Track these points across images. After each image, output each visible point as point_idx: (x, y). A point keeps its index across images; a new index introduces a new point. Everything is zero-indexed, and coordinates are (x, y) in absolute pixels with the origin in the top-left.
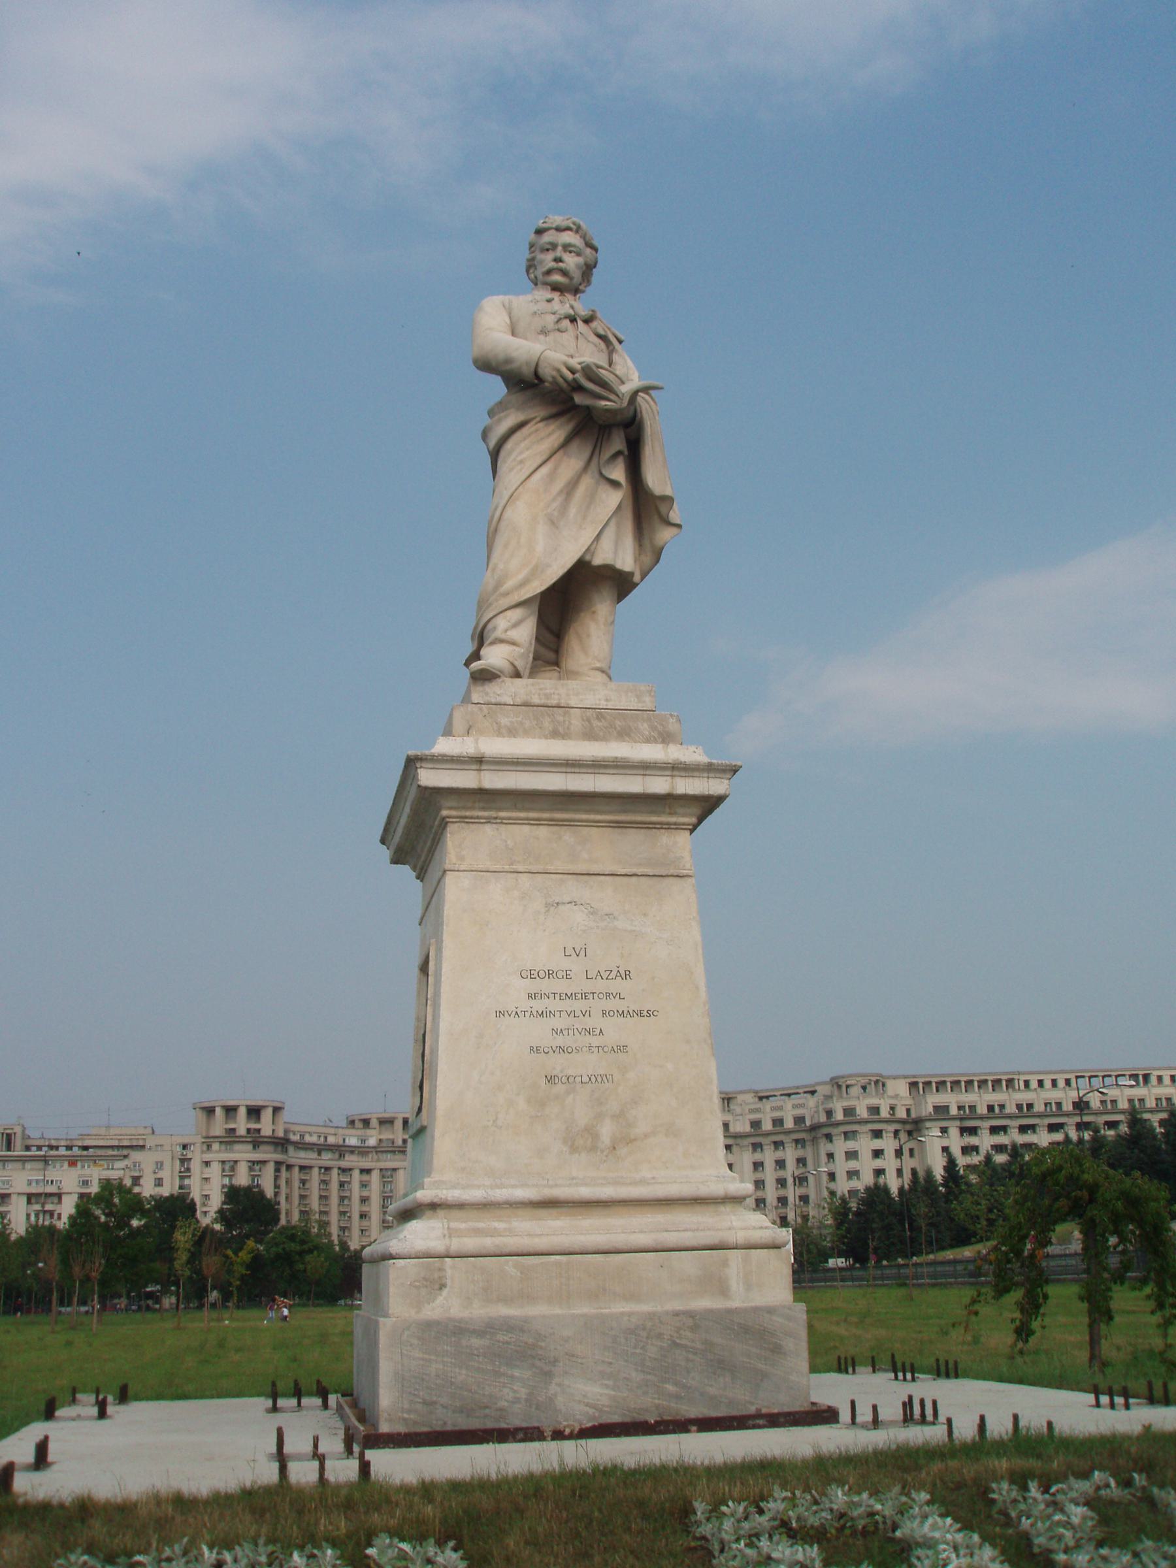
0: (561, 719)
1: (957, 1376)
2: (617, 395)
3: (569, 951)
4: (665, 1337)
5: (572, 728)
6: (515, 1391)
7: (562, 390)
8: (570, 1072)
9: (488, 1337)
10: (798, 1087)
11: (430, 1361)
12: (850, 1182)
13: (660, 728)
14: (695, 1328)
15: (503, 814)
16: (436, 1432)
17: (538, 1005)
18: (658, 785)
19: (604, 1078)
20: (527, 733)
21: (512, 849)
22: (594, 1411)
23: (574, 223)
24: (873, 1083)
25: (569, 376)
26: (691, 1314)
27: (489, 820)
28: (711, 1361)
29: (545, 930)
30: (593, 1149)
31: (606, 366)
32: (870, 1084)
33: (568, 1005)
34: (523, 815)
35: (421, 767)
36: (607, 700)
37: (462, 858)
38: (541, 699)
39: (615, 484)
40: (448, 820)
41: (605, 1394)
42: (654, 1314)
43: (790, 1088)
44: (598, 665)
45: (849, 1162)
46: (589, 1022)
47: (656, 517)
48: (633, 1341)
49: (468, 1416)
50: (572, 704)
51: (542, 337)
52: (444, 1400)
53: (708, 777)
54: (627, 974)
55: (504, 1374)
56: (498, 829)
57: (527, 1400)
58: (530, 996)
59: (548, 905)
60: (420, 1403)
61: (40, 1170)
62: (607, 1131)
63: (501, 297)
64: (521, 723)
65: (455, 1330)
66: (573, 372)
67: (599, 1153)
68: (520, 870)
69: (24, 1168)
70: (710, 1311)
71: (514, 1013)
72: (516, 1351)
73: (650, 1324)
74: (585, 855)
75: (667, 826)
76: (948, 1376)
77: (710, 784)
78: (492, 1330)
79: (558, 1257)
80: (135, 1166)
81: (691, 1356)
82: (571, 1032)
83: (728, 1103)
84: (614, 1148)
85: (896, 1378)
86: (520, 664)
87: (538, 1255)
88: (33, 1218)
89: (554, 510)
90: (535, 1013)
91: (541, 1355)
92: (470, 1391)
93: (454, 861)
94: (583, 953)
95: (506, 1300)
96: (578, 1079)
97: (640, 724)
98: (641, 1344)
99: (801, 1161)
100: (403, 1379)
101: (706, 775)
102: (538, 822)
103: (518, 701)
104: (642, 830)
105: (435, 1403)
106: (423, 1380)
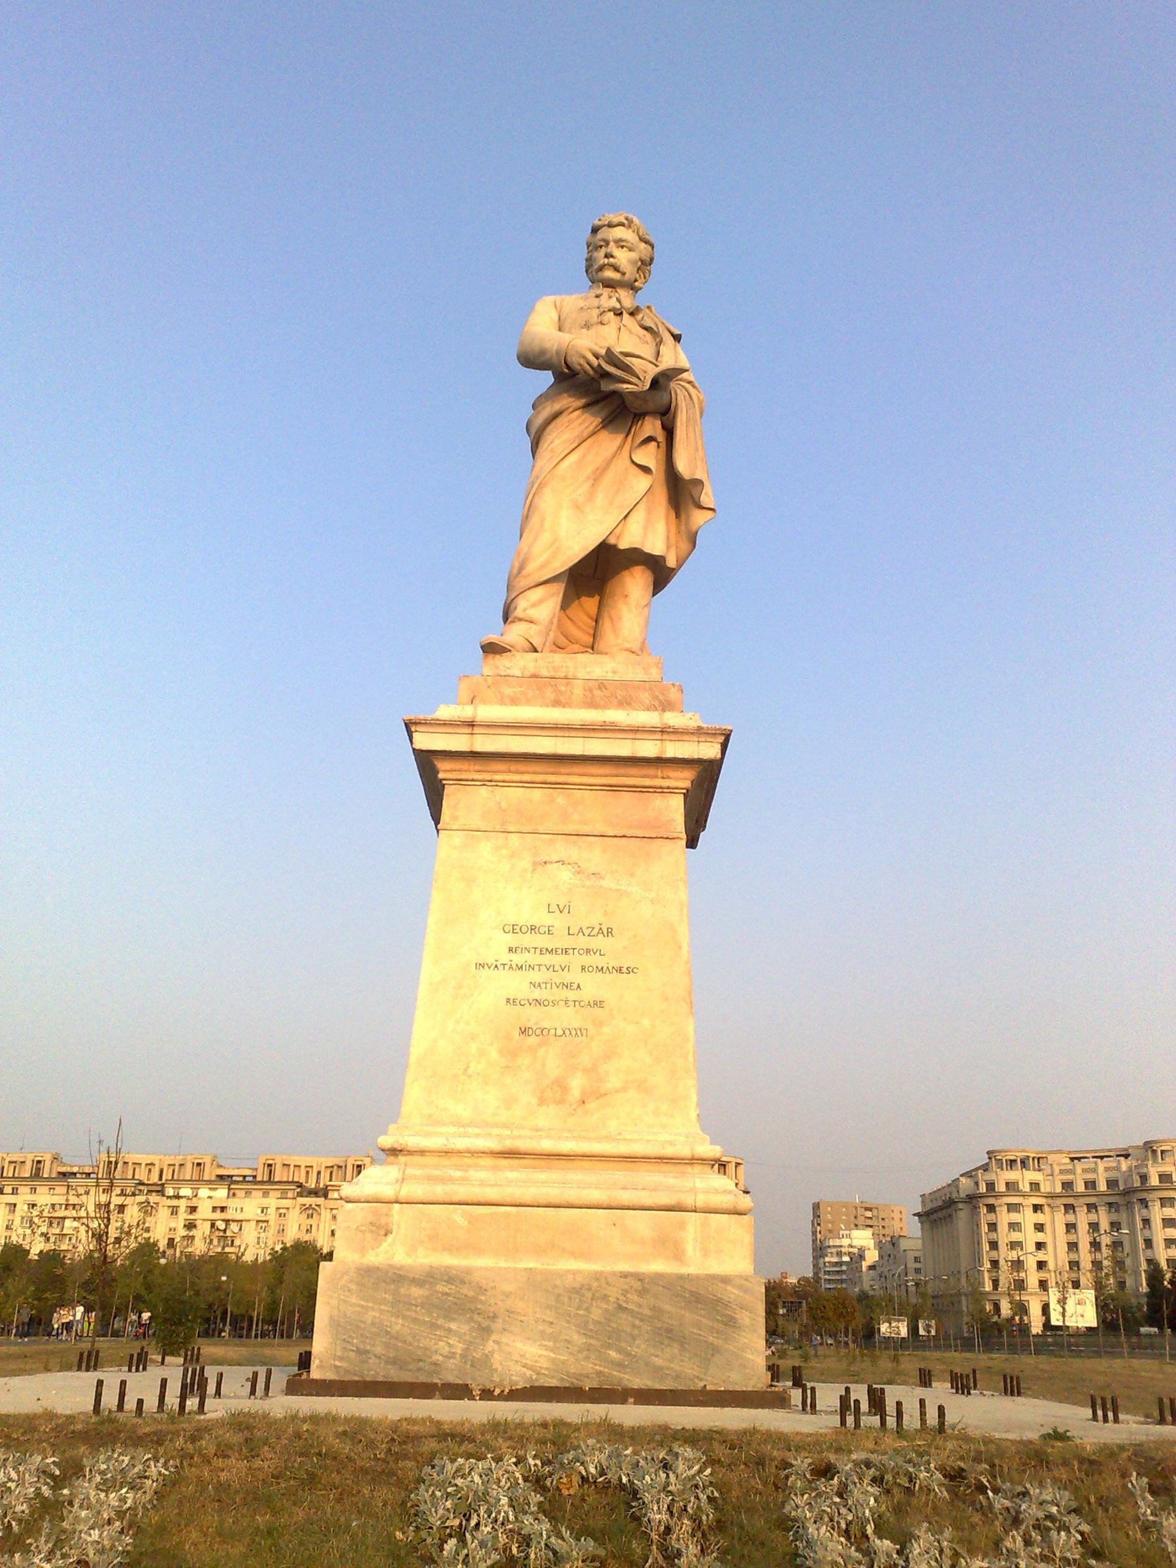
0: (563, 689)
1: (1019, 1394)
3: (554, 908)
4: (611, 1299)
6: (450, 1345)
8: (546, 1024)
9: (427, 1286)
10: (1110, 1150)
11: (367, 1308)
13: (661, 697)
14: (643, 1292)
15: (498, 777)
17: (517, 959)
18: (648, 748)
19: (581, 1031)
20: (528, 702)
21: (504, 811)
22: (531, 1372)
23: (627, 219)
25: (595, 362)
26: (639, 1277)
27: (484, 783)
28: (659, 1329)
29: (530, 887)
30: (561, 1102)
33: (548, 959)
35: (416, 731)
36: (614, 672)
38: (549, 672)
39: (645, 469)
41: (545, 1356)
42: (601, 1273)
43: (1102, 1151)
44: (627, 645)
46: (568, 977)
47: (691, 507)
48: (577, 1301)
51: (584, 330)
52: (379, 1350)
53: (699, 742)
56: (493, 792)
58: (510, 950)
59: (535, 864)
60: (353, 1351)
62: (577, 1084)
66: (597, 357)
70: (659, 1276)
71: (494, 966)
72: (456, 1304)
73: (596, 1284)
74: (576, 817)
75: (660, 790)
76: (1012, 1394)
77: (701, 748)
82: (549, 986)
83: (1039, 1163)
84: (584, 1102)
86: (536, 642)
87: (489, 1205)
89: (580, 495)
90: (514, 966)
91: (480, 1309)
92: (405, 1342)
94: (566, 910)
95: (450, 1249)
96: (553, 1032)
99: (1115, 1226)
100: (338, 1325)
103: (527, 673)
105: (367, 1352)
106: (358, 1327)
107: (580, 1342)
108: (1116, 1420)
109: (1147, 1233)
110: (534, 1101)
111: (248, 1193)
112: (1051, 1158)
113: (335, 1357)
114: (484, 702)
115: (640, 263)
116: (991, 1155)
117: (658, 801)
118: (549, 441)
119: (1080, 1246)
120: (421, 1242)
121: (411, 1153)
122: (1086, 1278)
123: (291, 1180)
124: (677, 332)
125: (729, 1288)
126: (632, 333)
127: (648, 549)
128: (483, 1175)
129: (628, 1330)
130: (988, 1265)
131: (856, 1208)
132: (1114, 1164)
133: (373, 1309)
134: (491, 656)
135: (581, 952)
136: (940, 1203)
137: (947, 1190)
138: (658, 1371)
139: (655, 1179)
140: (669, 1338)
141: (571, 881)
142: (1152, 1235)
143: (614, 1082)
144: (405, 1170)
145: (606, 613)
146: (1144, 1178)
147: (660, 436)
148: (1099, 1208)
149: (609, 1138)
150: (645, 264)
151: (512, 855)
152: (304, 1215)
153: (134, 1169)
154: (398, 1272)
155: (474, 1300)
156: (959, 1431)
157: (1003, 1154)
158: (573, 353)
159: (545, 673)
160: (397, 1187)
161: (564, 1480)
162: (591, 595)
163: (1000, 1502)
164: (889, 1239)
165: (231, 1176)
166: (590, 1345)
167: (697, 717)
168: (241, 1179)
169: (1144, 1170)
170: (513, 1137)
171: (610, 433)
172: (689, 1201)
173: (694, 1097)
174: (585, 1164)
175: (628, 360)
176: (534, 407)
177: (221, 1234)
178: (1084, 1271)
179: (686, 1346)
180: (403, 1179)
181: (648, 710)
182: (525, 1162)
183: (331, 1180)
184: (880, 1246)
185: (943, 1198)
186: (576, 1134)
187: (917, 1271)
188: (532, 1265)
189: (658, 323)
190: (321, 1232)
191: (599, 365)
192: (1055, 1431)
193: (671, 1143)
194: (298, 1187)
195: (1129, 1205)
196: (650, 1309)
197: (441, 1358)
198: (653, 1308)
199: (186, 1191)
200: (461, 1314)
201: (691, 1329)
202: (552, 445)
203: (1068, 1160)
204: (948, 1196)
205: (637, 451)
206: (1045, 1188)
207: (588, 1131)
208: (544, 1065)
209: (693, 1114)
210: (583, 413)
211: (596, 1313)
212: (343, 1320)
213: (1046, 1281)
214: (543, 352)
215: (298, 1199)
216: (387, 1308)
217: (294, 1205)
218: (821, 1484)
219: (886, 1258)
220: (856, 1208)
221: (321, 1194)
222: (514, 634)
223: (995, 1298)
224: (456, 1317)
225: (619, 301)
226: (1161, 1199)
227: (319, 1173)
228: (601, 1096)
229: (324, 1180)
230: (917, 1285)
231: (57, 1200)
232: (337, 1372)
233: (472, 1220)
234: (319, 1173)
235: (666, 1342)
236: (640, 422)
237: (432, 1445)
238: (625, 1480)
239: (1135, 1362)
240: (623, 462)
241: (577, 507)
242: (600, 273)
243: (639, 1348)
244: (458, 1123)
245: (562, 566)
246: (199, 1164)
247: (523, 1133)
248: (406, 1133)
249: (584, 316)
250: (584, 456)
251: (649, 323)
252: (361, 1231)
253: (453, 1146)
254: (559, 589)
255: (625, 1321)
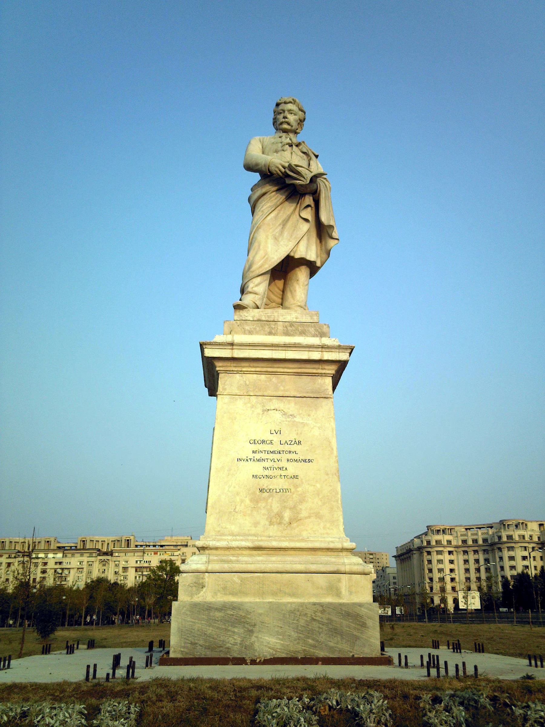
0: (274, 326)
1: (483, 652)
2: (304, 178)
5: (279, 330)
6: (235, 639)
7: (281, 177)
8: (271, 487)
10: (484, 525)
12: (511, 571)
13: (319, 330)
14: (323, 612)
15: (244, 369)
16: (196, 658)
17: (257, 456)
18: (316, 355)
20: (257, 333)
23: (293, 100)
24: (521, 524)
25: (283, 170)
26: (321, 605)
27: (238, 372)
28: (331, 629)
30: (280, 523)
31: (306, 167)
32: (519, 524)
33: (271, 456)
34: (253, 369)
36: (296, 318)
37: (225, 389)
39: (306, 220)
40: (219, 372)
42: (303, 603)
44: (299, 304)
45: (510, 562)
46: (281, 464)
47: (327, 235)
48: (293, 616)
49: (212, 651)
50: (280, 320)
51: (275, 154)
52: (201, 642)
54: (300, 442)
55: (229, 630)
57: (240, 644)
58: (253, 452)
59: (264, 411)
61: (141, 556)
62: (287, 515)
63: (258, 137)
64: (255, 329)
65: (208, 608)
66: (284, 168)
67: (283, 526)
68: (251, 395)
69: (134, 556)
76: (480, 652)
78: (225, 609)
79: (259, 574)
80: (183, 554)
81: (321, 626)
82: (272, 469)
83: (451, 531)
85: (530, 665)
86: (258, 303)
88: (138, 578)
90: (255, 460)
92: (213, 638)
93: (221, 390)
94: (279, 432)
95: (233, 594)
96: (274, 491)
97: (310, 328)
98: (297, 618)
99: (487, 561)
101: (338, 351)
102: (261, 373)
103: (255, 319)
104: (310, 377)
105: (197, 644)
106: (191, 632)
107: (295, 636)
108: (542, 666)
109: (501, 563)
110: (267, 523)
111: (73, 555)
112: (456, 529)
113: (181, 647)
114: (236, 333)
115: (299, 121)
116: (429, 528)
117: (320, 380)
118: (261, 206)
119: (471, 570)
120: (219, 591)
121: (211, 549)
122: (474, 586)
123: (94, 548)
124: (317, 154)
125: (362, 609)
126: (297, 155)
127: (308, 258)
128: (245, 559)
129: (317, 629)
130: (428, 580)
131: (365, 554)
132: (486, 531)
133: (198, 623)
134: (238, 311)
135: (287, 452)
136: (405, 551)
137: (408, 545)
138: (331, 649)
139: (326, 559)
140: (336, 633)
141: (281, 419)
142: (503, 564)
143: (304, 514)
144: (209, 557)
145: (288, 289)
146: (500, 537)
147: (313, 204)
148: (479, 552)
149: (303, 540)
150: (301, 121)
151: (252, 407)
152: (101, 565)
153: (15, 545)
154: (209, 605)
155: (244, 617)
156: (484, 676)
157: (434, 527)
158: (273, 165)
159: (263, 319)
160: (207, 565)
161: (322, 708)
162: (280, 279)
163: (519, 712)
164: (381, 568)
165: (64, 547)
166: (299, 637)
167: (337, 340)
168: (69, 548)
169: (500, 534)
170: (259, 541)
171: (290, 203)
172: (342, 569)
173: (342, 520)
174: (292, 552)
175: (299, 169)
176: (252, 190)
177: (60, 575)
178: (472, 582)
179: (344, 637)
180: (209, 561)
181: (314, 336)
182: (265, 552)
183: (114, 548)
184: (377, 572)
185: (406, 549)
186: (287, 539)
187: (395, 583)
188: (271, 600)
189: (309, 150)
190: (110, 573)
191: (285, 172)
192: (527, 675)
193: (332, 542)
194: (98, 551)
195: (493, 550)
196: (327, 620)
197: (230, 645)
198: (328, 619)
199: (41, 555)
200: (239, 624)
201: (346, 629)
202: (262, 209)
203: (464, 530)
204: (409, 547)
205: (302, 211)
206: (454, 543)
207: (293, 537)
208: (271, 506)
209: (342, 527)
210: (277, 194)
211: (302, 622)
212: (184, 629)
213: (455, 587)
214: (257, 165)
215: (98, 557)
216: (204, 622)
217: (96, 560)
218: (437, 706)
219: (380, 578)
220: (365, 554)
221: (109, 554)
222: (248, 300)
223: (431, 595)
224: (237, 625)
225: (291, 139)
226: (507, 547)
227: (108, 544)
228: (299, 520)
229: (111, 548)
230: (395, 590)
231: (138, 559)
232: (182, 654)
233: (242, 580)
234: (108, 544)
235: (334, 634)
236: (303, 198)
237: (254, 693)
238: (349, 707)
239: (500, 625)
240: (296, 217)
241: (276, 238)
242: (281, 126)
243: (322, 638)
244: (232, 534)
245: (269, 267)
246: (48, 542)
247: (263, 538)
248: (209, 539)
249: (274, 147)
250: (278, 214)
251: (305, 151)
252: (190, 586)
253: (231, 545)
254: (268, 277)
255: (315, 625)
